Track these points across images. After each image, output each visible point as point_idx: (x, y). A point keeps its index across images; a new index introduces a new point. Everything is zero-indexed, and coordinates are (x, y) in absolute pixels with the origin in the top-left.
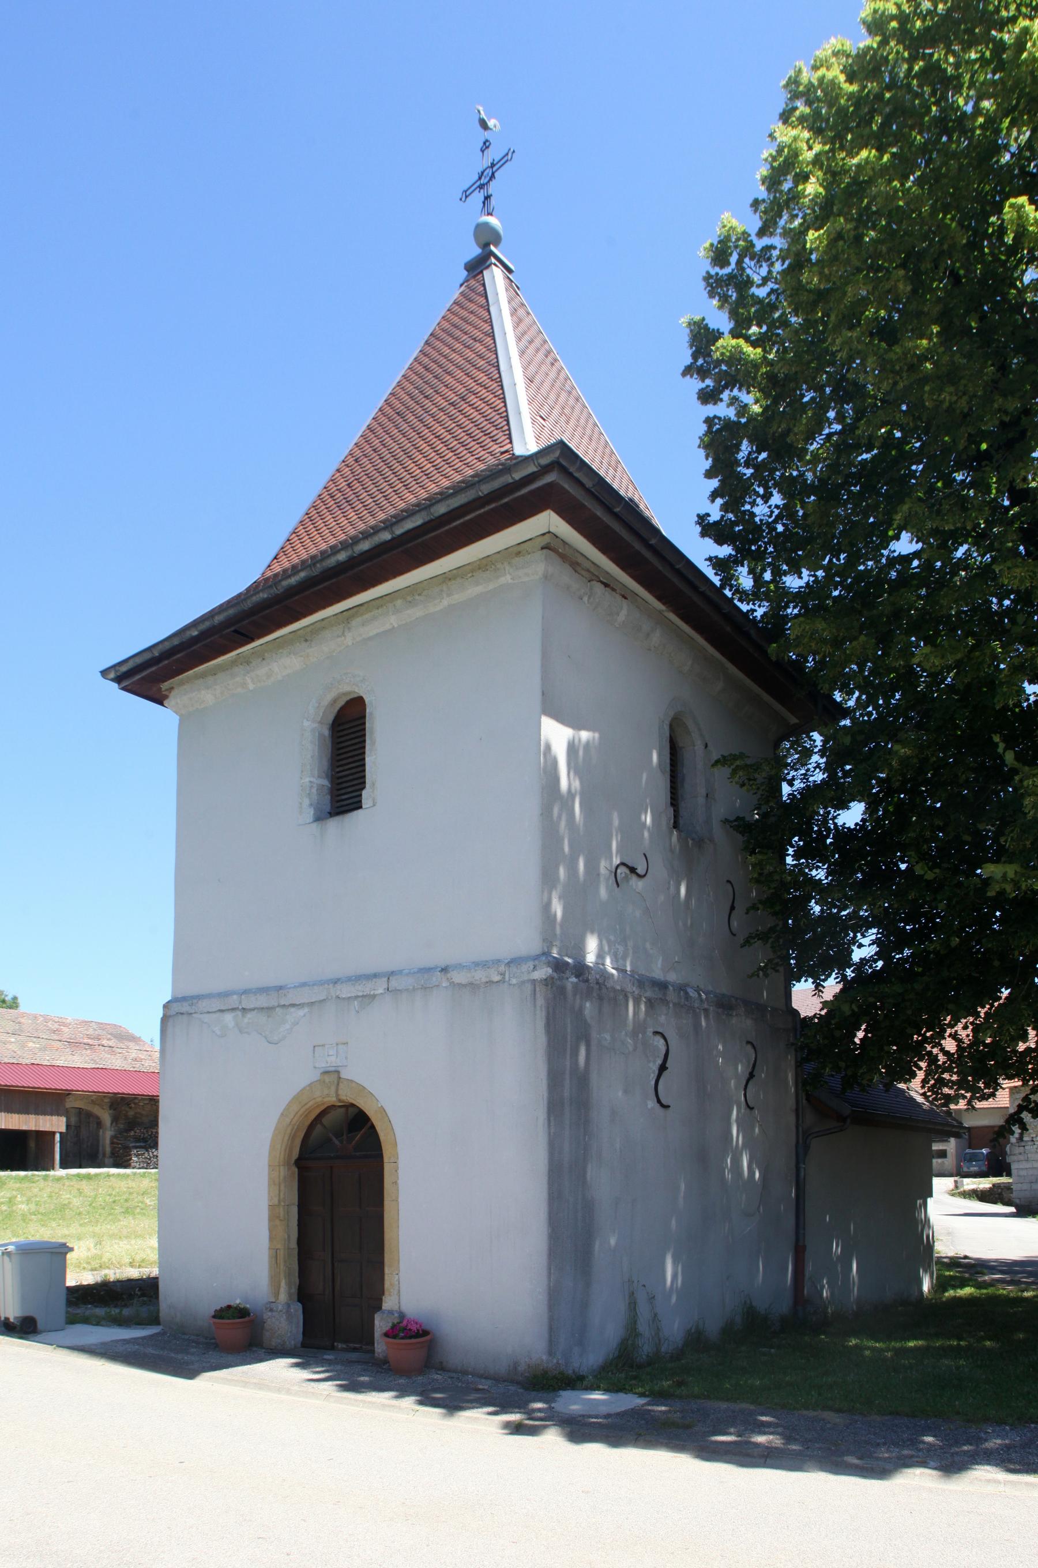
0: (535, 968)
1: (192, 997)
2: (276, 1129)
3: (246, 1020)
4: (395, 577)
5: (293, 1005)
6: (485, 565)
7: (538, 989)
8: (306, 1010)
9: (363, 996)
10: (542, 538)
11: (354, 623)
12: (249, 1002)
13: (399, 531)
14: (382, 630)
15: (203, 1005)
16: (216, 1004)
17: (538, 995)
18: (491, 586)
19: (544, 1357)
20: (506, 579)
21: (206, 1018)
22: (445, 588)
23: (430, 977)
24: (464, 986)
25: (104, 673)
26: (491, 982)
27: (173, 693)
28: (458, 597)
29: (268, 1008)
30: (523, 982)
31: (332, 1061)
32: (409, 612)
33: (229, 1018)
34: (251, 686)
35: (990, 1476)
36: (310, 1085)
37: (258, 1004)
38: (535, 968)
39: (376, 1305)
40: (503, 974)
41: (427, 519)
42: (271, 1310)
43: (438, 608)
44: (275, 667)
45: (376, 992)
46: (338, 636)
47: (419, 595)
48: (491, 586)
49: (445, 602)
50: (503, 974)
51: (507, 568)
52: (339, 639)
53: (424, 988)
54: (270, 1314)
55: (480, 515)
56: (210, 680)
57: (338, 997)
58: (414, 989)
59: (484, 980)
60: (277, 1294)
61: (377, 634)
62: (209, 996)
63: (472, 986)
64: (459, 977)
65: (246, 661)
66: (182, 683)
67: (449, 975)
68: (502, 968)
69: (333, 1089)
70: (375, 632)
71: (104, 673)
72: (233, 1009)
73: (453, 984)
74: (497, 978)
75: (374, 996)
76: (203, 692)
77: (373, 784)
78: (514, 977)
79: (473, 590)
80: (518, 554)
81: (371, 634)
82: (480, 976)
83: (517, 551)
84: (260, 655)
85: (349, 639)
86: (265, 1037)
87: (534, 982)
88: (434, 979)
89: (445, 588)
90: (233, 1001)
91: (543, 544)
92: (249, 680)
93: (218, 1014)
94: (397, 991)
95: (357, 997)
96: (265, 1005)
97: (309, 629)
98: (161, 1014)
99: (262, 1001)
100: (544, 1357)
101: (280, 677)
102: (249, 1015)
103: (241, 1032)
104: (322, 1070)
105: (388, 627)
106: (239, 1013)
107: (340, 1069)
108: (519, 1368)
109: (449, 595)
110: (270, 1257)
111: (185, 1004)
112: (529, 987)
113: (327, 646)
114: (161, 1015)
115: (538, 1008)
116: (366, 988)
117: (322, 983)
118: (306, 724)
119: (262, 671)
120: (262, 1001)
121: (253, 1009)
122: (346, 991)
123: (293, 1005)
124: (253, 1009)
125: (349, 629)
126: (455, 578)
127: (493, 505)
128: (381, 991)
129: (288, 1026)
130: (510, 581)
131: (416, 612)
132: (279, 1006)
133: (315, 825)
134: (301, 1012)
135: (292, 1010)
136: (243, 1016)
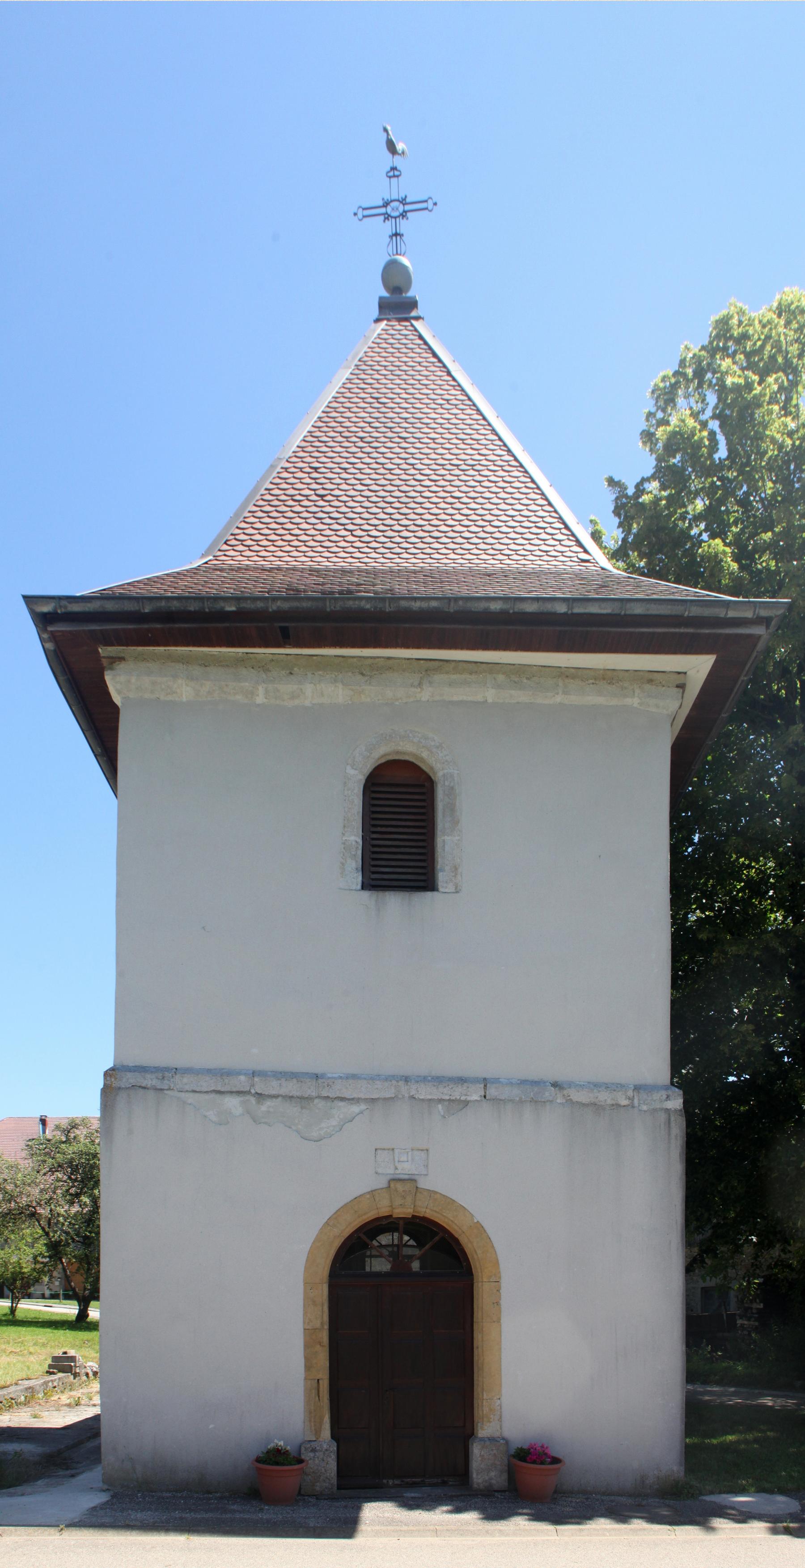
0: (668, 1098)
1: (167, 1069)
2: (317, 1239)
3: (264, 1108)
4: (516, 650)
5: (342, 1099)
6: (609, 677)
7: (672, 1119)
8: (363, 1107)
9: (449, 1100)
10: (676, 676)
11: (438, 678)
12: (273, 1086)
13: (577, 610)
14: (470, 699)
15: (186, 1081)
16: (207, 1083)
17: (673, 1124)
18: (614, 702)
19: (675, 1468)
20: (634, 702)
21: (191, 1098)
22: (561, 684)
23: (537, 1092)
24: (584, 1105)
25: (29, 600)
26: (618, 1106)
27: (122, 666)
28: (574, 699)
29: (301, 1098)
30: (655, 1110)
31: (406, 1168)
32: (513, 692)
33: (233, 1103)
34: (260, 699)
35: (604, 1526)
36: (372, 1192)
37: (283, 1091)
38: (668, 1098)
39: (466, 1431)
40: (631, 1099)
41: (617, 611)
42: (314, 1450)
43: (546, 702)
44: (309, 689)
45: (469, 1098)
46: (412, 685)
47: (527, 678)
48: (614, 702)
49: (558, 699)
50: (631, 1099)
51: (637, 691)
52: (413, 689)
53: (533, 1101)
54: (312, 1455)
55: (675, 634)
56: (197, 671)
57: (412, 1097)
58: (521, 1101)
59: (609, 1102)
60: (318, 1431)
61: (462, 702)
62: (188, 1071)
63: (596, 1107)
64: (578, 1096)
65: (263, 666)
66: (143, 658)
67: (565, 1092)
68: (630, 1093)
69: (409, 1199)
70: (460, 698)
71: (29, 600)
72: (239, 1093)
73: (570, 1102)
74: (624, 1102)
75: (466, 1103)
76: (180, 681)
77: (455, 869)
78: (644, 1103)
79: (593, 699)
80: (650, 681)
81: (455, 698)
82: (604, 1097)
83: (649, 678)
84: (289, 668)
85: (426, 694)
86: (298, 1132)
87: (667, 1111)
88: (547, 1094)
89: (561, 684)
90: (242, 1082)
91: (678, 682)
92: (261, 690)
93: (213, 1095)
94: (497, 1101)
95: (440, 1101)
96: (295, 1093)
97: (370, 661)
98: (100, 1084)
99: (291, 1088)
100: (675, 1468)
101: (307, 703)
102: (269, 1103)
103: (255, 1120)
104: (389, 1177)
105: (479, 698)
106: (253, 1100)
107: (416, 1177)
108: (647, 1482)
109: (565, 693)
110: (307, 1391)
111: (148, 1076)
112: (663, 1116)
113: (396, 691)
114: (102, 1086)
115: (673, 1136)
116: (457, 1092)
117: (389, 1078)
118: (351, 771)
119: (287, 687)
120: (291, 1088)
121: (276, 1097)
122: (425, 1092)
123: (342, 1099)
124: (276, 1097)
125: (430, 682)
126: (574, 677)
127: (691, 630)
128: (475, 1097)
129: (334, 1122)
130: (635, 705)
131: (521, 696)
132: (319, 1097)
133: (366, 894)
134: (355, 1109)
135: (341, 1104)
136: (258, 1102)
